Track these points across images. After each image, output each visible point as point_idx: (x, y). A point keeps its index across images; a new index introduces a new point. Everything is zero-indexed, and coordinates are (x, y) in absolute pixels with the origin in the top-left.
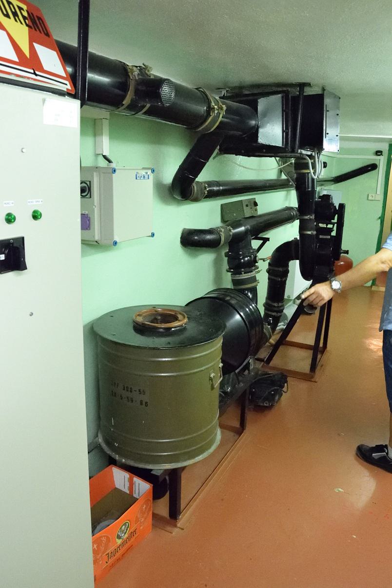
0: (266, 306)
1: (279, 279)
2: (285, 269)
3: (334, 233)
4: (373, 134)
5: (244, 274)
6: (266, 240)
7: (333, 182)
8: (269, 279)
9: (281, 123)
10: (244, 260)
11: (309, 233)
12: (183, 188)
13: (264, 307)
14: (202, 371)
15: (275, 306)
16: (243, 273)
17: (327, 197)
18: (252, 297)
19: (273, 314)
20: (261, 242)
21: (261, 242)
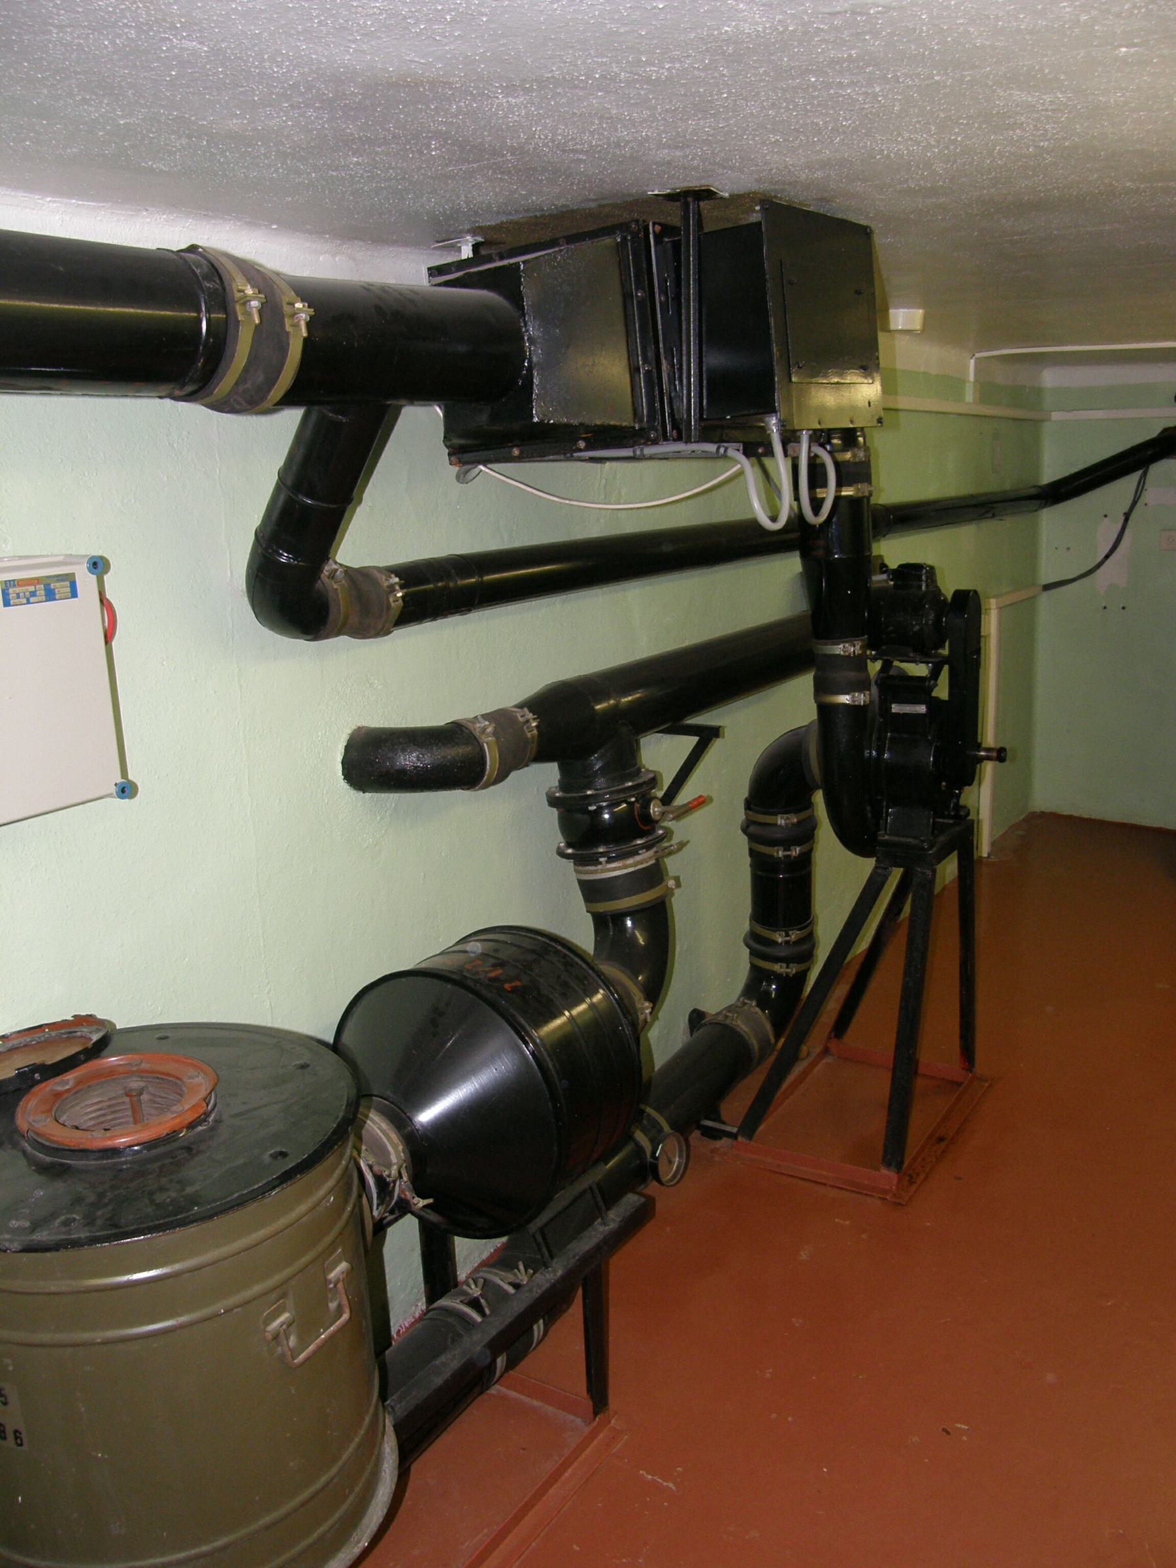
0: (752, 943)
1: (781, 854)
2: (804, 815)
3: (942, 692)
4: (1145, 340)
5: (607, 862)
6: (707, 735)
7: (1038, 502)
8: (752, 852)
9: (620, 328)
10: (629, 803)
11: (845, 699)
12: (295, 584)
13: (748, 946)
14: (93, 1344)
15: (775, 943)
16: (602, 860)
17: (909, 573)
18: (941, 856)
19: (778, 968)
20: (692, 741)
21: (692, 741)
